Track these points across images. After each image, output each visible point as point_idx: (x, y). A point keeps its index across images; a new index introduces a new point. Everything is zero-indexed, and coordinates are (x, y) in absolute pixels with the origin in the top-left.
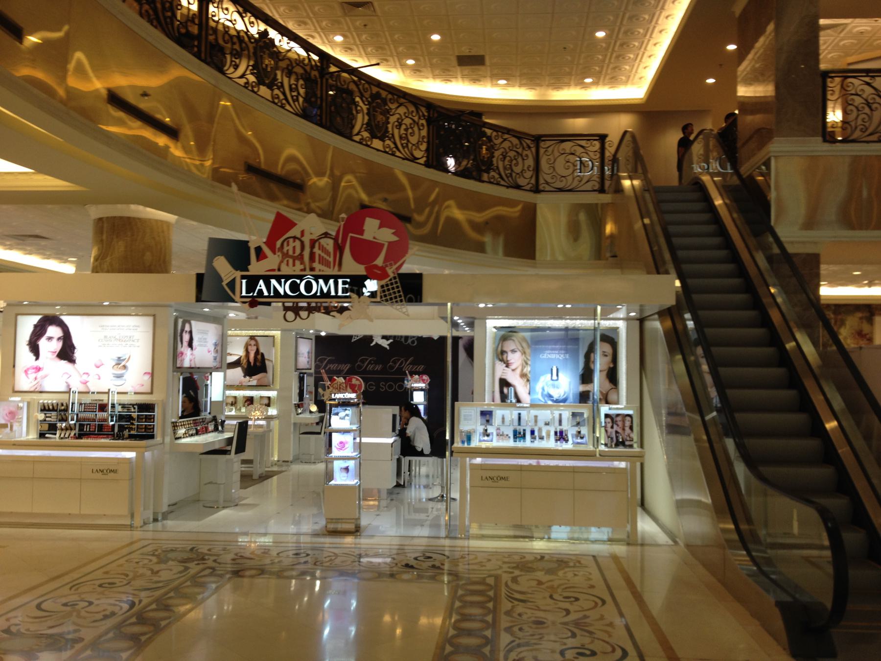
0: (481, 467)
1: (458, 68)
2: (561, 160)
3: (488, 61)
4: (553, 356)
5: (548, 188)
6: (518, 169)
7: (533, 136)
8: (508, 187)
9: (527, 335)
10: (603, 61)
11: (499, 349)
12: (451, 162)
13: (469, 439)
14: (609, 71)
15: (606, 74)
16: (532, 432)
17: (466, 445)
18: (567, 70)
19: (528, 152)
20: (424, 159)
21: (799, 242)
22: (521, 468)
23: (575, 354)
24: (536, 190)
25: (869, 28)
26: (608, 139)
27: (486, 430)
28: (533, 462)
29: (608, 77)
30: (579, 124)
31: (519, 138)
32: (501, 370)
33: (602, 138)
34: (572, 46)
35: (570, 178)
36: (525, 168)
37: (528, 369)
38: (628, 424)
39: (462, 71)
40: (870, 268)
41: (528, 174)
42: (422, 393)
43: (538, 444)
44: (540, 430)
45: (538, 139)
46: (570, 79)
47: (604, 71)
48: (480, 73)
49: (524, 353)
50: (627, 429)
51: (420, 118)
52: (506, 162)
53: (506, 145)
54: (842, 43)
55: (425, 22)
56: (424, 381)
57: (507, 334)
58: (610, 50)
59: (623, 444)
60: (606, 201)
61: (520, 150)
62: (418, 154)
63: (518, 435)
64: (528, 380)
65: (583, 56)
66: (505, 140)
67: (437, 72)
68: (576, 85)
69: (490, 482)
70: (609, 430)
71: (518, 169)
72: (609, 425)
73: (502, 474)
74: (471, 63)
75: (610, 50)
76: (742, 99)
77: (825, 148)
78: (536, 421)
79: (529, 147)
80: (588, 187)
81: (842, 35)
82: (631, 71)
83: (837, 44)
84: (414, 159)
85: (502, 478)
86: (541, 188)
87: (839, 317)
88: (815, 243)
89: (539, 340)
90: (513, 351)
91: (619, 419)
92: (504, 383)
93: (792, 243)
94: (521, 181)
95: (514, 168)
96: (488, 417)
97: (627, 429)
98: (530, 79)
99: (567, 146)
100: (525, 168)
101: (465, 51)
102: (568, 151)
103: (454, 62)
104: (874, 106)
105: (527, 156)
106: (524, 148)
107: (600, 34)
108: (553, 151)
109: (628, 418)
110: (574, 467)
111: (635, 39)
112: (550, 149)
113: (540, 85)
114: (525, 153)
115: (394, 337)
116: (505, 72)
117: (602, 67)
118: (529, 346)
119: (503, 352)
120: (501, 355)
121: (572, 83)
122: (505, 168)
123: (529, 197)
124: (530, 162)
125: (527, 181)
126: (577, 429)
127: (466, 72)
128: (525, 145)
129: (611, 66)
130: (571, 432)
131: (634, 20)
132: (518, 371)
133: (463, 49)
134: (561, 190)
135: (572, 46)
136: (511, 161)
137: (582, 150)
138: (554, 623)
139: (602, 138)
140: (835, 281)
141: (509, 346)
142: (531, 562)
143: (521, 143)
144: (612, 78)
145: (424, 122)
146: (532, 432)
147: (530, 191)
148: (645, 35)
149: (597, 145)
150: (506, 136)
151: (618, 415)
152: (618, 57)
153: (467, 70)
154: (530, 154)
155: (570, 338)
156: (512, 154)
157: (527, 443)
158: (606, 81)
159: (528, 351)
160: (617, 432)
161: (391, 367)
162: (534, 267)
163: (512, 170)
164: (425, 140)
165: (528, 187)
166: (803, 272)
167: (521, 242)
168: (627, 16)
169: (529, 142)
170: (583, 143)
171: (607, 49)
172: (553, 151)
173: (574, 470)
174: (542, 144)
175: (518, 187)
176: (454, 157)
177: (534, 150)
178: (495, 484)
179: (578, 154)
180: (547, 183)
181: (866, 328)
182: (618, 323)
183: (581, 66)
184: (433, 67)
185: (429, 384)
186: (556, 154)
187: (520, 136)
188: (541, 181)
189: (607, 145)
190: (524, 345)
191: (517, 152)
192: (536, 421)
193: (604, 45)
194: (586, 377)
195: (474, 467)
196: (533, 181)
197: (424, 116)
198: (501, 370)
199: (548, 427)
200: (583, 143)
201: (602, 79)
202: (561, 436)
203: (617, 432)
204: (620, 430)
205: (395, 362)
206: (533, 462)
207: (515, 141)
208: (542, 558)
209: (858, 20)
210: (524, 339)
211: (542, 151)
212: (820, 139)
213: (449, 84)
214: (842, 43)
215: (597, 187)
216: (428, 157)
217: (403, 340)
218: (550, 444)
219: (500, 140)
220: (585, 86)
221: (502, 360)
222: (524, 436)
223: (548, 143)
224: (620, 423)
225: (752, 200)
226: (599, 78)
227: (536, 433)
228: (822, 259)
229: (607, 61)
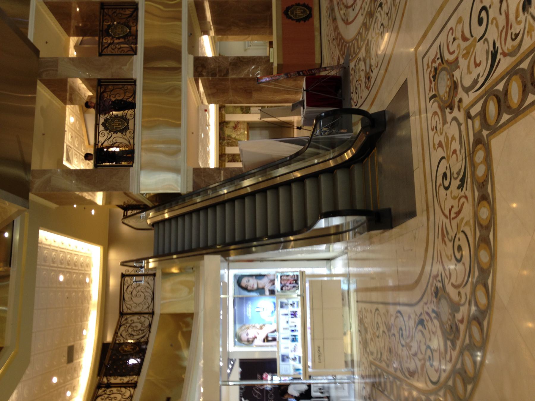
0: (313, 361)
1: (75, 362)
2: (135, 300)
3: (70, 344)
4: (250, 310)
5: (151, 307)
6: (139, 326)
7: (120, 317)
8: (150, 332)
9: (238, 326)
10: (77, 273)
11: (246, 343)
12: (132, 361)
13: (298, 370)
14: (83, 269)
15: (86, 271)
16: (293, 331)
17: (301, 372)
18: (80, 294)
19: (129, 319)
20: (131, 389)
21: (187, 179)
22: (313, 339)
23: (248, 299)
24: (152, 314)
25: (70, 133)
26: (124, 273)
27: (293, 359)
28: (309, 331)
29: (86, 269)
30: (114, 282)
31: (120, 326)
32: (259, 341)
33: (123, 276)
34: (67, 294)
35: (146, 294)
36: (139, 321)
37: (258, 326)
38: (285, 278)
39: (77, 359)
40: (200, 130)
41: (142, 319)
42: (274, 377)
43: (299, 328)
44: (291, 327)
45: (122, 314)
46: (86, 291)
47: (83, 272)
48: (78, 347)
49: (248, 328)
50: (288, 278)
51: (105, 394)
52: (134, 333)
53: (124, 334)
54: (77, 146)
55: (45, 388)
56: (267, 377)
57: (239, 339)
58: (71, 271)
59: (296, 281)
60: (161, 273)
61: (128, 325)
62: (128, 394)
63: (294, 339)
64: (264, 325)
65: (73, 286)
66: (121, 335)
67: (76, 375)
68: (90, 287)
69: (322, 358)
70: (289, 288)
71: (139, 326)
72: (286, 288)
73: (316, 349)
74: (71, 354)
75: (71, 271)
76: (104, 202)
77: (137, 166)
78: (286, 329)
79: (126, 319)
80: (151, 283)
81: (72, 146)
82: (84, 256)
83: (77, 148)
84: (131, 396)
85: (319, 350)
86: (151, 311)
87: (226, 138)
88: (187, 170)
89: (240, 319)
90: (247, 334)
91: (283, 282)
92: (266, 339)
93: (187, 188)
94: (147, 324)
95: (139, 328)
96: (285, 358)
97: (288, 278)
98: (83, 315)
99: (127, 296)
100: (139, 321)
101: (64, 359)
102: (130, 296)
103: (71, 365)
104: (115, 141)
105: (131, 321)
106: (127, 323)
107: (61, 278)
108: (130, 305)
109: (282, 277)
110: (310, 309)
111: (66, 257)
112: (128, 306)
113: (88, 308)
114: (130, 322)
115: (241, 397)
116: (78, 334)
117: (80, 273)
118: (244, 325)
119: (248, 341)
120: (250, 342)
121: (88, 289)
122: (138, 334)
123: (156, 318)
124: (135, 318)
125: (147, 320)
126: (289, 306)
127: (77, 357)
128: (125, 322)
129: (80, 268)
130: (290, 309)
131: (55, 260)
132: (260, 331)
133: (63, 361)
134: (153, 299)
135: (67, 294)
136: (134, 330)
137: (130, 288)
138: (389, 342)
139: (123, 276)
140: (206, 160)
141: (244, 337)
142: (362, 338)
143: (124, 325)
144: (87, 266)
145: (108, 390)
146: (293, 331)
147: (152, 317)
148: (64, 252)
149: (127, 279)
150: (119, 334)
151: (281, 283)
152: (75, 265)
153: (76, 356)
154: (130, 318)
155: (240, 302)
156: (130, 330)
157: (299, 334)
158: (89, 269)
159: (247, 326)
160: (290, 283)
161: (259, 396)
162: (198, 313)
163: (140, 330)
164: (119, 389)
165: (150, 319)
166: (201, 174)
167: (182, 324)
168: (52, 265)
169: (123, 319)
170: (125, 287)
171: (70, 273)
172: (130, 305)
173: (312, 309)
174: (125, 311)
175: (150, 325)
176: (128, 360)
177: (128, 316)
178: (322, 354)
179: (132, 290)
180: (148, 307)
181: (232, 125)
182: (229, 275)
183: (79, 286)
184: (73, 378)
185: (268, 373)
186: (131, 302)
187: (119, 325)
188: (147, 311)
189: (128, 273)
190: (244, 328)
191: (129, 326)
192: (286, 329)
193: (68, 275)
194: (261, 291)
195: (314, 367)
196: (146, 316)
197: (104, 391)
198: (259, 341)
199: (290, 322)
200: (125, 287)
201: (86, 272)
202: (294, 314)
203: (290, 283)
204: (289, 282)
205: (256, 394)
206: (309, 331)
207: (122, 328)
208: (359, 331)
209: (65, 141)
210: (241, 328)
211: (129, 311)
212: (131, 168)
213: (83, 367)
214: (77, 146)
215: (152, 278)
216: (130, 387)
217: (242, 391)
218: (298, 321)
219: (121, 338)
220: (91, 281)
221: (253, 341)
222: (295, 336)
223: (125, 307)
224: (285, 282)
225: (163, 200)
226: (87, 274)
227: (293, 329)
228: (196, 167)
229: (77, 271)
